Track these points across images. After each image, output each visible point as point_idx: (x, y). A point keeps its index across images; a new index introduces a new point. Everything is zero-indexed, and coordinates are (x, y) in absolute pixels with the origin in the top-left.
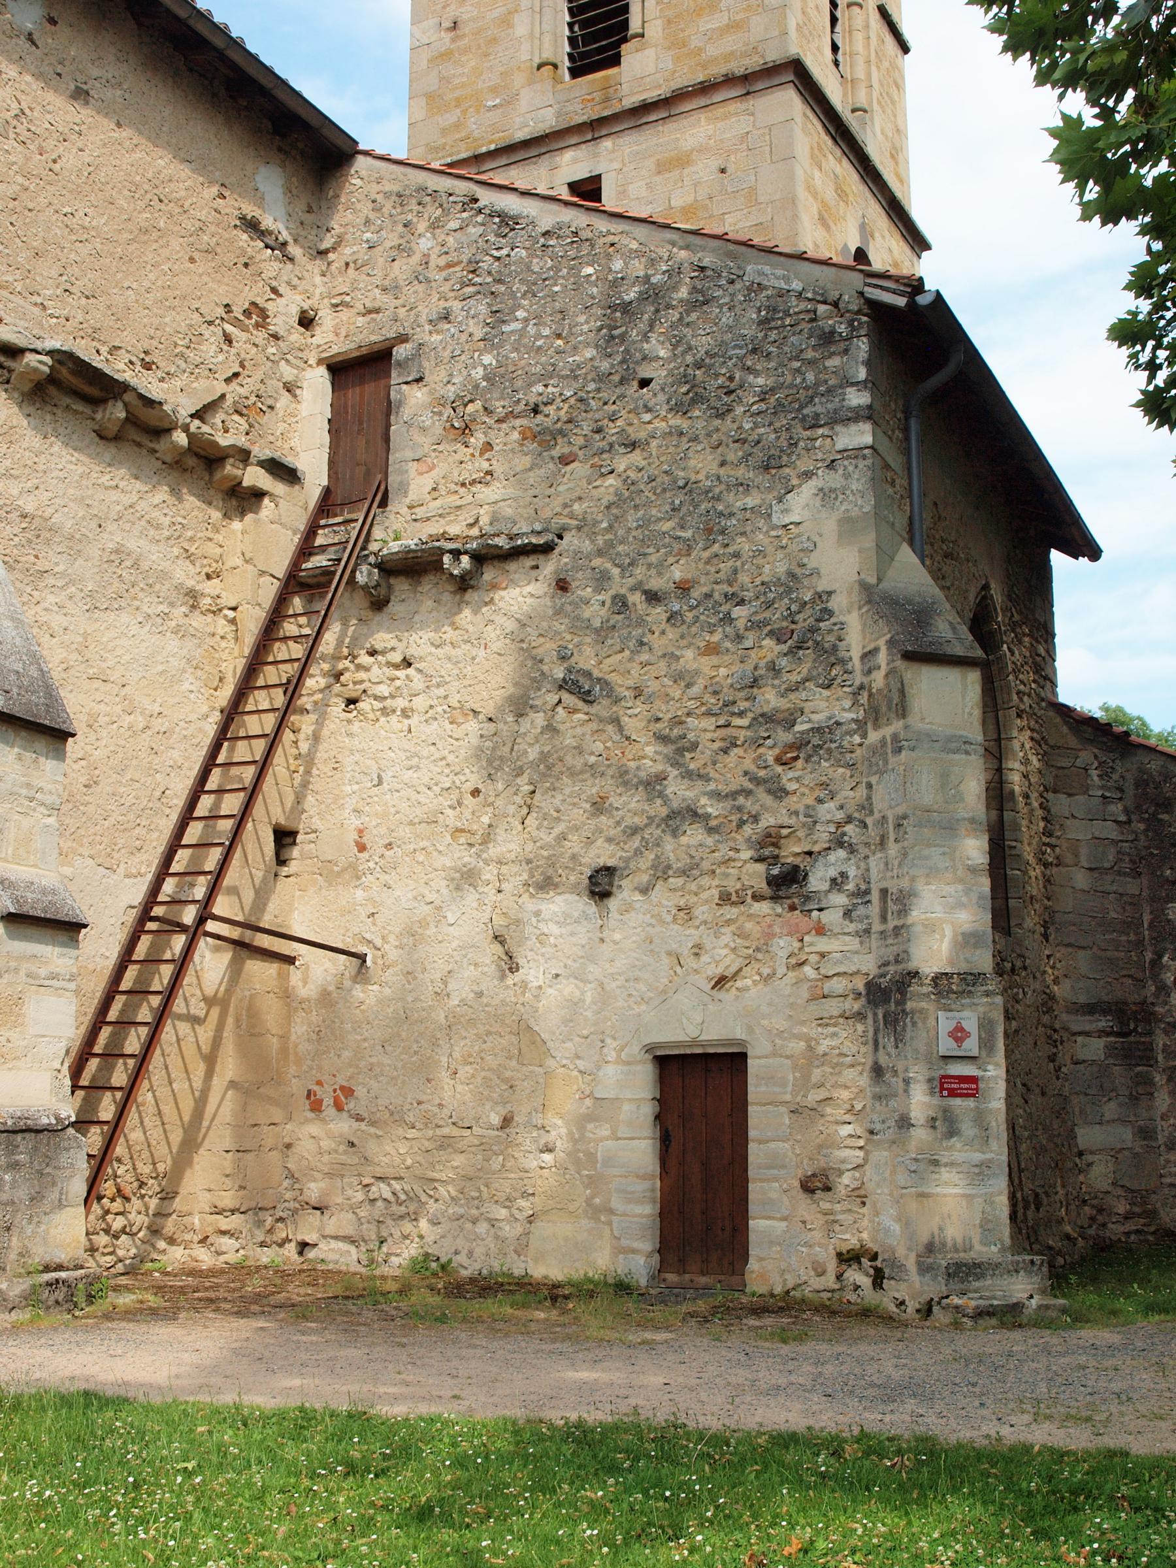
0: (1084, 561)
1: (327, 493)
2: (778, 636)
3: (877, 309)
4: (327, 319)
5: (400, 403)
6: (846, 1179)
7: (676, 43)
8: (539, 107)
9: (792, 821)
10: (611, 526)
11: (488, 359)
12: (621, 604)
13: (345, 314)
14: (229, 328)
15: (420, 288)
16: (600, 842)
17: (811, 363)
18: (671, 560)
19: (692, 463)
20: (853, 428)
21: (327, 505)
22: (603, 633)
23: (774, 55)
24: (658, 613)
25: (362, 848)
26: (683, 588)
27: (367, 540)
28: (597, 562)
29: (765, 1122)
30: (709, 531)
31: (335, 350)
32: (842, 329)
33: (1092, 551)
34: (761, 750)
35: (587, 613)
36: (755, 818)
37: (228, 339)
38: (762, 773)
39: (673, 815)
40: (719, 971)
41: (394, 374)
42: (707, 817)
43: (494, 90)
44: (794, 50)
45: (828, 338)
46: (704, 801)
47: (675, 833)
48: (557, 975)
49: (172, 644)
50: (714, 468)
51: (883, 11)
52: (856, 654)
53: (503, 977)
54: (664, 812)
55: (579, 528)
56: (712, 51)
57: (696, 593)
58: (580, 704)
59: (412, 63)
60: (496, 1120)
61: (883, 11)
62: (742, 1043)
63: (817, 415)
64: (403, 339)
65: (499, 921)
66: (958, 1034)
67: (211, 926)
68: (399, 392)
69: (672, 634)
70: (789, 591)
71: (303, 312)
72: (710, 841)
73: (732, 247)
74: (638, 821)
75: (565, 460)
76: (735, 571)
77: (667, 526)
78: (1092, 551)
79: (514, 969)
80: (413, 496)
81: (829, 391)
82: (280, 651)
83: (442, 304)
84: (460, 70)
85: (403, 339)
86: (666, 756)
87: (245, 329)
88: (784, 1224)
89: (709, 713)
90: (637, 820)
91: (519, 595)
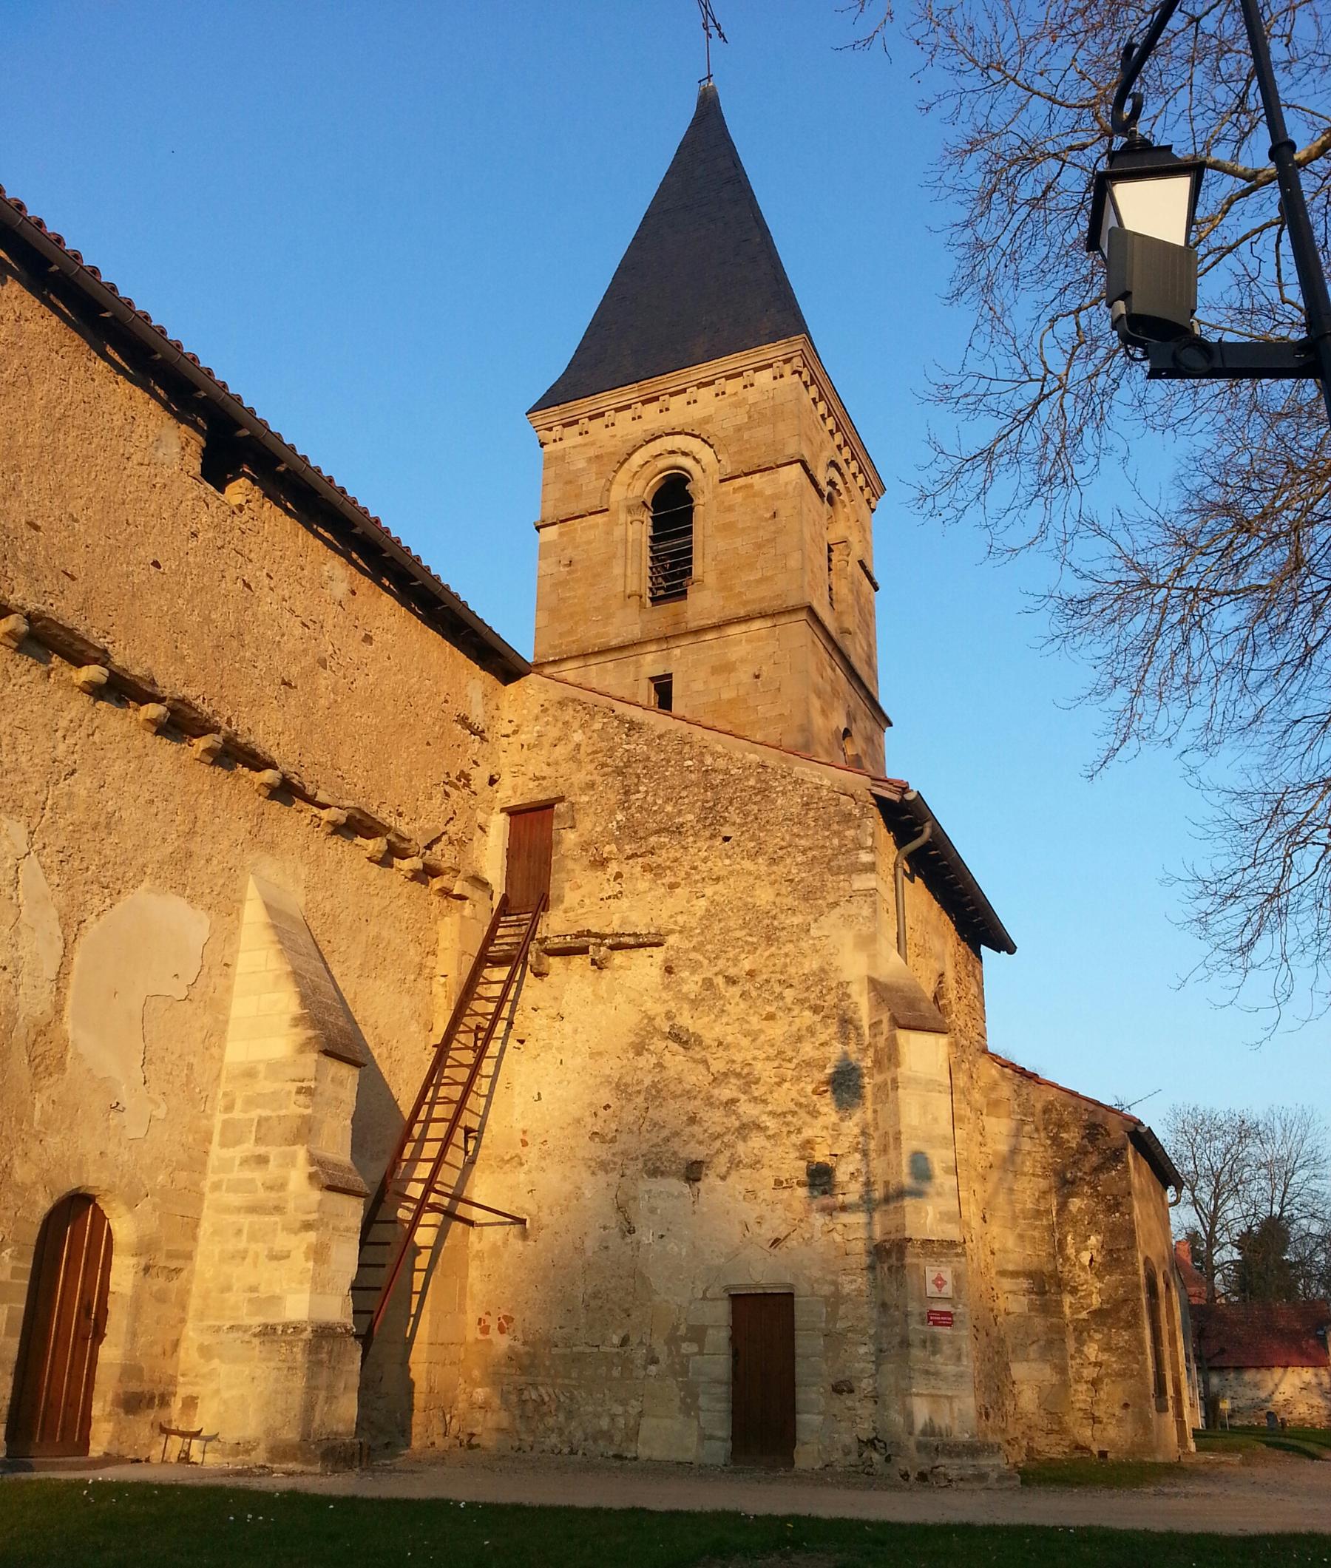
0: (1004, 953)
1: (505, 900)
2: (816, 1009)
3: (882, 803)
4: (506, 781)
5: (559, 843)
6: (864, 1383)
7: (725, 588)
8: (626, 624)
9: (824, 1134)
10: (703, 932)
11: (619, 817)
12: (708, 984)
13: (520, 780)
14: (448, 788)
15: (574, 766)
16: (692, 1143)
17: (836, 833)
18: (743, 956)
19: (758, 892)
20: (864, 876)
21: (505, 907)
22: (695, 1003)
23: (792, 602)
24: (735, 991)
25: (525, 1143)
26: (751, 974)
27: (534, 933)
28: (693, 955)
29: (807, 1344)
30: (769, 938)
31: (513, 803)
32: (856, 812)
33: (1011, 949)
34: (802, 1084)
35: (685, 989)
36: (799, 1131)
37: (447, 794)
38: (803, 1100)
39: (743, 1126)
40: (775, 1235)
41: (555, 822)
42: (766, 1128)
43: (597, 609)
44: (808, 599)
45: (847, 818)
46: (764, 1117)
47: (745, 1140)
48: (662, 1236)
49: (406, 1000)
50: (771, 898)
51: (861, 563)
52: (865, 1024)
53: (624, 1237)
54: (737, 1124)
55: (680, 932)
56: (749, 596)
57: (760, 979)
58: (681, 1050)
59: (539, 588)
60: (616, 1340)
61: (861, 563)
62: (791, 1286)
63: (840, 867)
64: (561, 799)
65: (621, 1197)
66: (939, 1282)
67: (433, 1198)
68: (559, 835)
69: (743, 1005)
70: (822, 980)
71: (492, 776)
72: (768, 1145)
73: (784, 754)
74: (719, 1129)
75: (672, 886)
76: (785, 965)
77: (738, 934)
78: (1011, 949)
79: (632, 1231)
80: (566, 904)
81: (847, 851)
82: (478, 1006)
83: (589, 777)
84: (572, 594)
85: (561, 799)
86: (739, 1087)
87: (457, 788)
88: (821, 1417)
89: (768, 1058)
90: (718, 1129)
91: (641, 970)
